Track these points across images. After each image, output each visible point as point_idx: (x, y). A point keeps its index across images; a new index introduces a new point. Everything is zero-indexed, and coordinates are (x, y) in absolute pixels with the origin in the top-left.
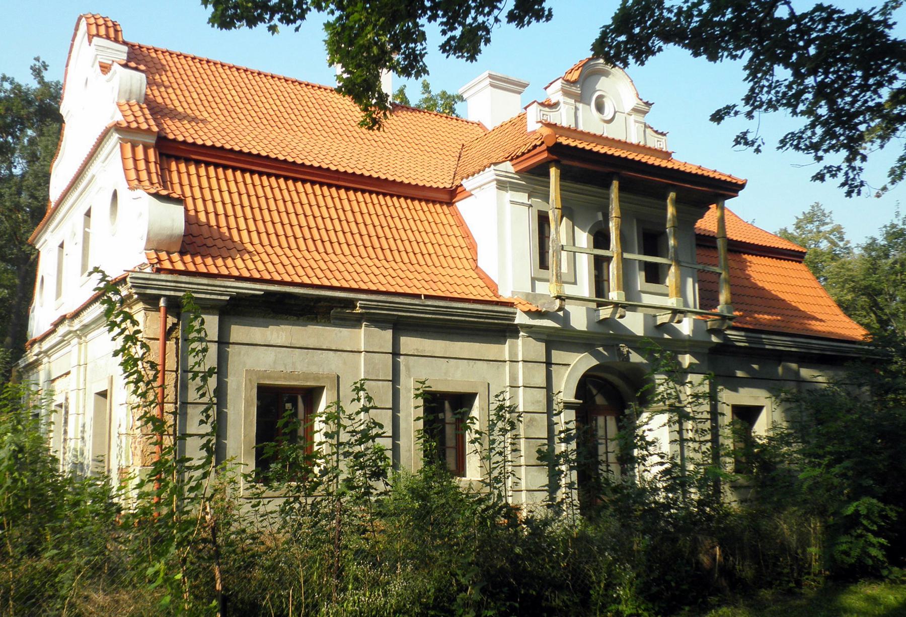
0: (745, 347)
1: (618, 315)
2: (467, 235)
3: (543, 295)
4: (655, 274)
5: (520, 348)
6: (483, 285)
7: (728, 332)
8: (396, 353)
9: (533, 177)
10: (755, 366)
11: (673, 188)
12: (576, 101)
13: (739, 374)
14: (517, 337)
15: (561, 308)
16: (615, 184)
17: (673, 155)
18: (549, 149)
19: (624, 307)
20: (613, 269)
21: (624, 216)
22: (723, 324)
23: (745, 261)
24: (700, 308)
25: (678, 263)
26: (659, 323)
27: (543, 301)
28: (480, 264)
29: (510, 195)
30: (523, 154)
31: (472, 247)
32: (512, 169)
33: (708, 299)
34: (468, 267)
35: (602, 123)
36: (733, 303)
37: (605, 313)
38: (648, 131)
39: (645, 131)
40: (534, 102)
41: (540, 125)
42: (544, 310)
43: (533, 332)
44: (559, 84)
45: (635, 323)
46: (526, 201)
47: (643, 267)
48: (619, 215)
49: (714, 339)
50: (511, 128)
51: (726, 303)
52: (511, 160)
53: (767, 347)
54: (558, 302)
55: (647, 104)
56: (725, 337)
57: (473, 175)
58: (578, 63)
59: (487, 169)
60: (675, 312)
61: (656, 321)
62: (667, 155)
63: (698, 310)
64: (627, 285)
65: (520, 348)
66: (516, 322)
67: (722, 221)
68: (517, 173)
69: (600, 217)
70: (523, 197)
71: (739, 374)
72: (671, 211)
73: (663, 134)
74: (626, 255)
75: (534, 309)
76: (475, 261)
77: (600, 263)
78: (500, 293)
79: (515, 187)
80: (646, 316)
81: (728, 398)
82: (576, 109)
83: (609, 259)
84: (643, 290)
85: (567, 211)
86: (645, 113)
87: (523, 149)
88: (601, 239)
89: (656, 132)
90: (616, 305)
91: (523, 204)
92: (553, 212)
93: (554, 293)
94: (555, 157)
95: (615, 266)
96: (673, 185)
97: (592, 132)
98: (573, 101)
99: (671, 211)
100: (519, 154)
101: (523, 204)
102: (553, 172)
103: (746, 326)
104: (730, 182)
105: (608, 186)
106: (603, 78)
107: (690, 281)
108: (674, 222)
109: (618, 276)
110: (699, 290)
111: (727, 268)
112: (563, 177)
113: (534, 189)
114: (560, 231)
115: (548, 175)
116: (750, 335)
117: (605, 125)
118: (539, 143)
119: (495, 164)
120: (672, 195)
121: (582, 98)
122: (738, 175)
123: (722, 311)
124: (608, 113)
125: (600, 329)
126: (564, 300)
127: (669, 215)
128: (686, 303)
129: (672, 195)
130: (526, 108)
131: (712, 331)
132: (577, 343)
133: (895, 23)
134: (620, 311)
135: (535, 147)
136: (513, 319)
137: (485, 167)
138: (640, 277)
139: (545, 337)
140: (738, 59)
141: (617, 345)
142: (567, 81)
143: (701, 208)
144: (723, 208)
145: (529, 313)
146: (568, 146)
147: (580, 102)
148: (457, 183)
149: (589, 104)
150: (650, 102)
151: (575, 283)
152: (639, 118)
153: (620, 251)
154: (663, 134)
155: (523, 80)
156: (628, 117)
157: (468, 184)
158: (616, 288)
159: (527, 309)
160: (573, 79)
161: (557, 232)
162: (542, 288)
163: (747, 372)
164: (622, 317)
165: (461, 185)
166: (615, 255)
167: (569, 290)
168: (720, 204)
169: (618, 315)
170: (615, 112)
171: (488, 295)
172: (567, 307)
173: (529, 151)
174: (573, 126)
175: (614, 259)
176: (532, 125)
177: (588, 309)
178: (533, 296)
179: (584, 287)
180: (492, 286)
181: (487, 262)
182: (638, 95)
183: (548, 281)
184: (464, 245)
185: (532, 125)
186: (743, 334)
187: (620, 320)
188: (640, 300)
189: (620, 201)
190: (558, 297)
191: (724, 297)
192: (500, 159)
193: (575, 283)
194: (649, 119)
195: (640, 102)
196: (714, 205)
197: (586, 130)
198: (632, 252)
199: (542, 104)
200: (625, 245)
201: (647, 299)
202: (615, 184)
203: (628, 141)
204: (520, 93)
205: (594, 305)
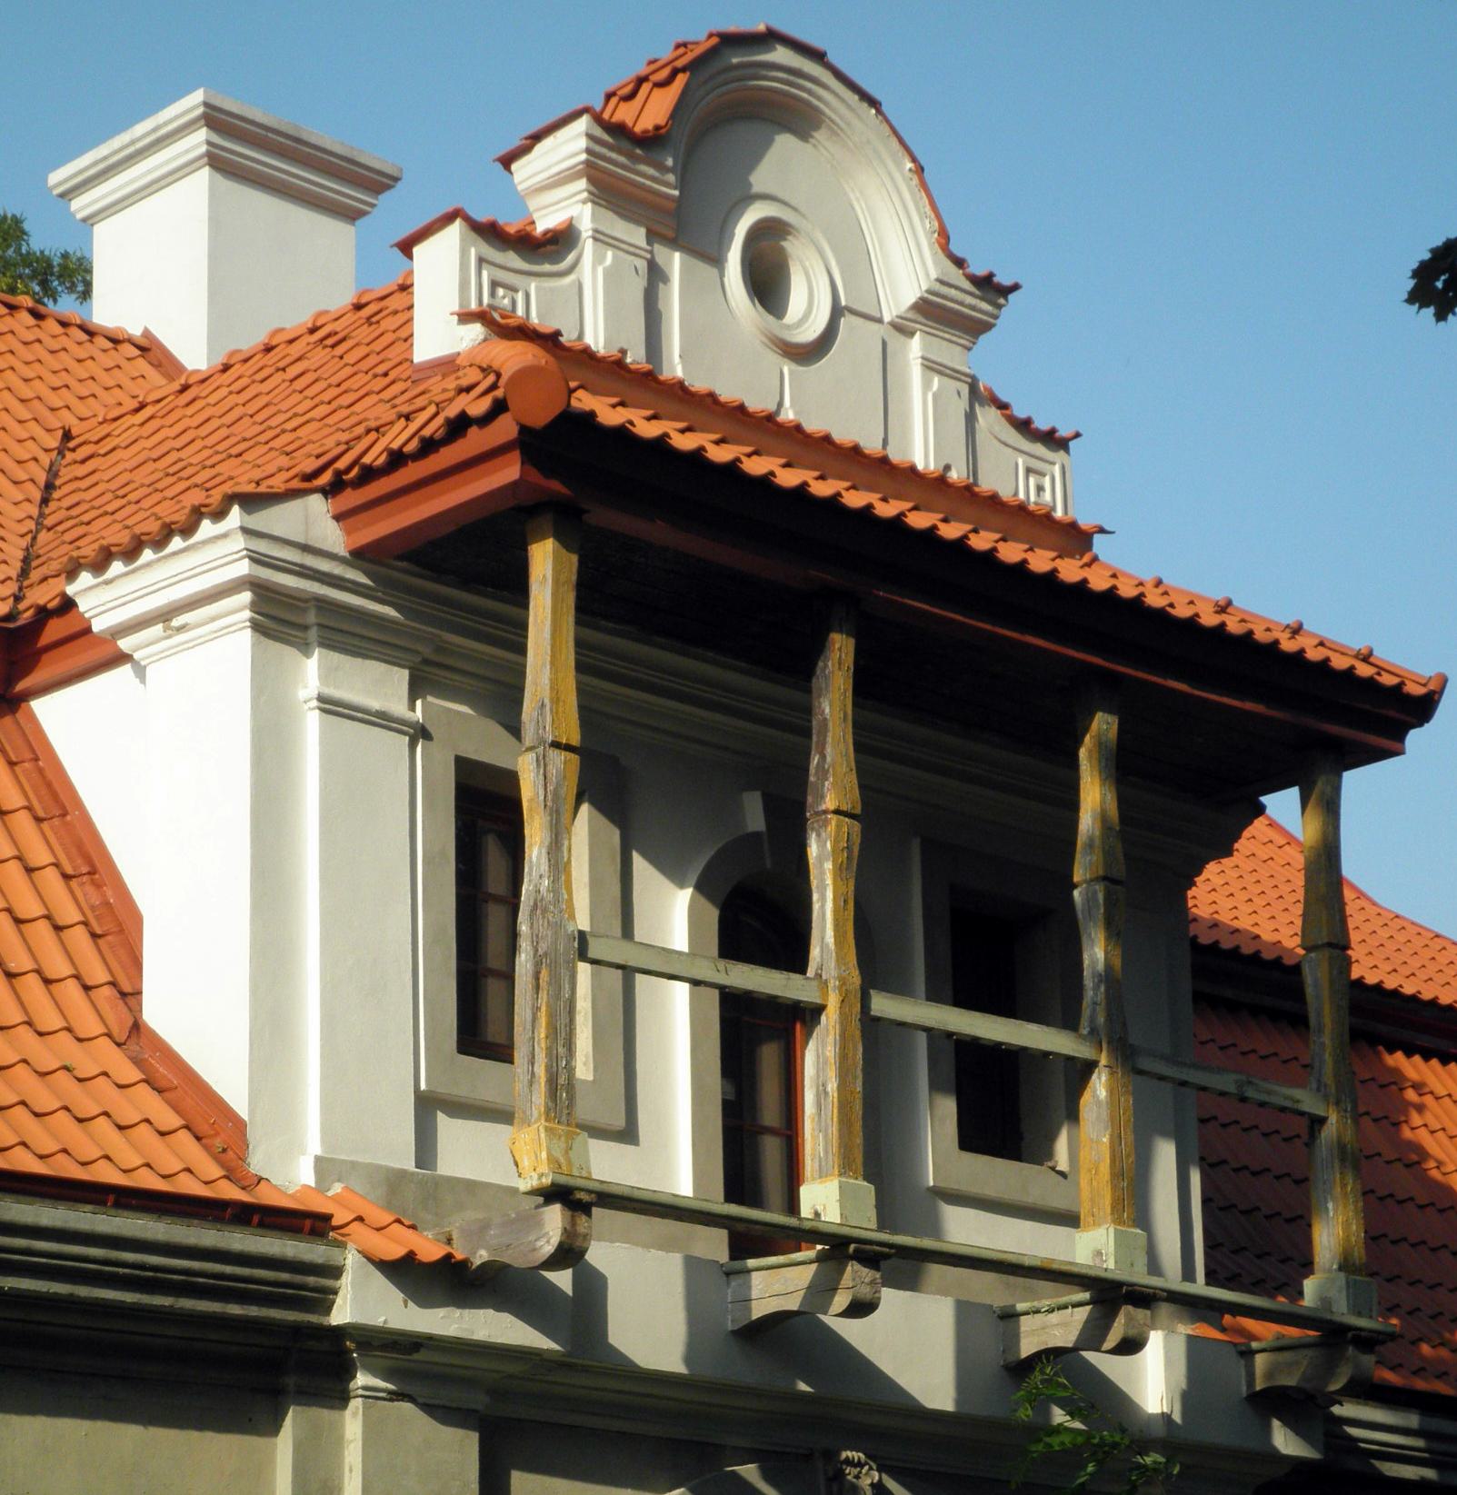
0: (1422, 1484)
1: (841, 1301)
2: (89, 864)
3: (471, 1186)
4: (1005, 1110)
5: (353, 1455)
6: (170, 1120)
9: (427, 581)
11: (1113, 692)
12: (652, 236)
14: (339, 1398)
15: (569, 1254)
16: (840, 652)
17: (1099, 542)
18: (531, 443)
19: (872, 1256)
20: (821, 1063)
21: (877, 818)
22: (1329, 1370)
23: (1396, 1081)
24: (1212, 1278)
25: (1127, 1056)
26: (1027, 1348)
27: (472, 1215)
28: (154, 1013)
29: (312, 672)
30: (397, 459)
31: (116, 927)
32: (333, 537)
33: (1250, 1239)
34: (91, 1026)
35: (773, 359)
36: (1373, 1264)
37: (776, 1286)
38: (988, 418)
39: (970, 418)
40: (448, 219)
41: (476, 331)
42: (481, 1256)
43: (421, 1372)
44: (571, 144)
45: (913, 1346)
46: (399, 707)
47: (961, 1072)
48: (852, 800)
49: (1285, 1441)
50: (320, 355)
51: (1346, 1265)
52: (331, 491)
54: (554, 1219)
55: (988, 286)
56: (1333, 1435)
57: (131, 554)
58: (665, 53)
59: (207, 528)
60: (1109, 1296)
61: (1013, 1338)
62: (1076, 538)
63: (1200, 1287)
64: (878, 1151)
65: (353, 1455)
66: (342, 1314)
67: (1325, 865)
68: (360, 556)
69: (754, 817)
70: (383, 686)
72: (1094, 797)
73: (1053, 440)
74: (883, 1005)
75: (430, 1250)
76: (130, 996)
77: (750, 1040)
78: (258, 1162)
79: (344, 633)
80: (965, 1311)
82: (656, 275)
83: (808, 1015)
84: (950, 1184)
85: (605, 779)
86: (974, 328)
87: (398, 437)
88: (758, 917)
89: (1024, 426)
90: (839, 1249)
91: (383, 720)
92: (542, 762)
93: (535, 1174)
94: (556, 486)
95: (831, 1052)
96: (1111, 681)
97: (727, 393)
98: (638, 236)
99: (1094, 797)
100: (376, 457)
101: (383, 720)
102: (546, 563)
103: (1421, 1384)
104: (1370, 683)
105: (800, 667)
106: (784, 143)
107: (1166, 1154)
108: (1108, 854)
109: (844, 1106)
110: (1206, 1201)
111: (1346, 1093)
112: (593, 601)
113: (440, 649)
114: (566, 857)
115: (516, 586)
117: (787, 368)
118: (479, 408)
119: (251, 501)
120: (1103, 725)
121: (684, 224)
122: (1410, 653)
123: (1326, 1302)
124: (806, 308)
125: (746, 1370)
126: (585, 1208)
127: (1087, 822)
128: (1154, 1267)
129: (1103, 725)
130: (406, 247)
131: (1272, 1402)
134: (855, 1277)
135: (459, 425)
136: (324, 1299)
137: (197, 514)
138: (937, 1123)
139: (479, 1401)
141: (830, 1455)
142: (618, 131)
143: (1224, 813)
144: (1331, 809)
145: (406, 1272)
146: (622, 434)
147: (673, 243)
148: (42, 595)
149: (716, 260)
150: (1003, 279)
151: (628, 1134)
152: (951, 354)
153: (855, 979)
154: (1053, 440)
155: (375, 155)
156: (895, 340)
157: (102, 600)
158: (833, 1161)
159: (395, 1252)
160: (646, 124)
161: (559, 867)
162: (469, 1151)
164: (861, 1308)
165: (68, 605)
166: (833, 1003)
167: (607, 1165)
168: (1321, 785)
169: (841, 1301)
170: (837, 312)
171: (199, 1175)
172: (598, 1255)
173: (429, 446)
174: (636, 356)
175: (830, 1019)
176: (439, 332)
177: (693, 1266)
178: (419, 1189)
179: (674, 1151)
180: (214, 1125)
181: (195, 1000)
182: (944, 237)
183: (503, 1116)
184: (69, 914)
185: (439, 332)
186: (1413, 1420)
187: (852, 1331)
188: (935, 1229)
189: (861, 747)
190: (557, 1194)
191: (1333, 1232)
192: (278, 483)
193: (628, 1134)
194: (989, 359)
195: (956, 275)
196: (1293, 794)
197: (699, 383)
198: (900, 988)
199: (490, 232)
200: (875, 960)
201: (965, 1229)
202: (840, 652)
203: (895, 456)
204: (351, 215)
205: (714, 1245)
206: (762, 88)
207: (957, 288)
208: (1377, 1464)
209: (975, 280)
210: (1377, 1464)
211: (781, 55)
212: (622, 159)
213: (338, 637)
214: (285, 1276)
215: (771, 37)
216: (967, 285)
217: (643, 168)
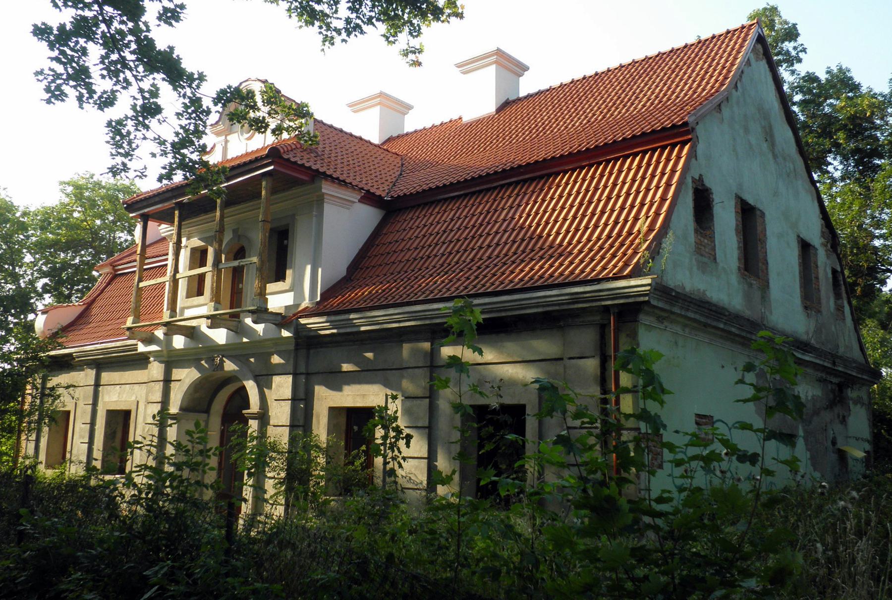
0: (332, 334)
7: (303, 321)
8: (97, 385)
10: (370, 355)
13: (346, 367)
53: (363, 329)
71: (346, 367)
81: (326, 399)
116: (333, 318)
132: (189, 360)
133: (290, 16)
140: (313, 32)
163: (356, 364)
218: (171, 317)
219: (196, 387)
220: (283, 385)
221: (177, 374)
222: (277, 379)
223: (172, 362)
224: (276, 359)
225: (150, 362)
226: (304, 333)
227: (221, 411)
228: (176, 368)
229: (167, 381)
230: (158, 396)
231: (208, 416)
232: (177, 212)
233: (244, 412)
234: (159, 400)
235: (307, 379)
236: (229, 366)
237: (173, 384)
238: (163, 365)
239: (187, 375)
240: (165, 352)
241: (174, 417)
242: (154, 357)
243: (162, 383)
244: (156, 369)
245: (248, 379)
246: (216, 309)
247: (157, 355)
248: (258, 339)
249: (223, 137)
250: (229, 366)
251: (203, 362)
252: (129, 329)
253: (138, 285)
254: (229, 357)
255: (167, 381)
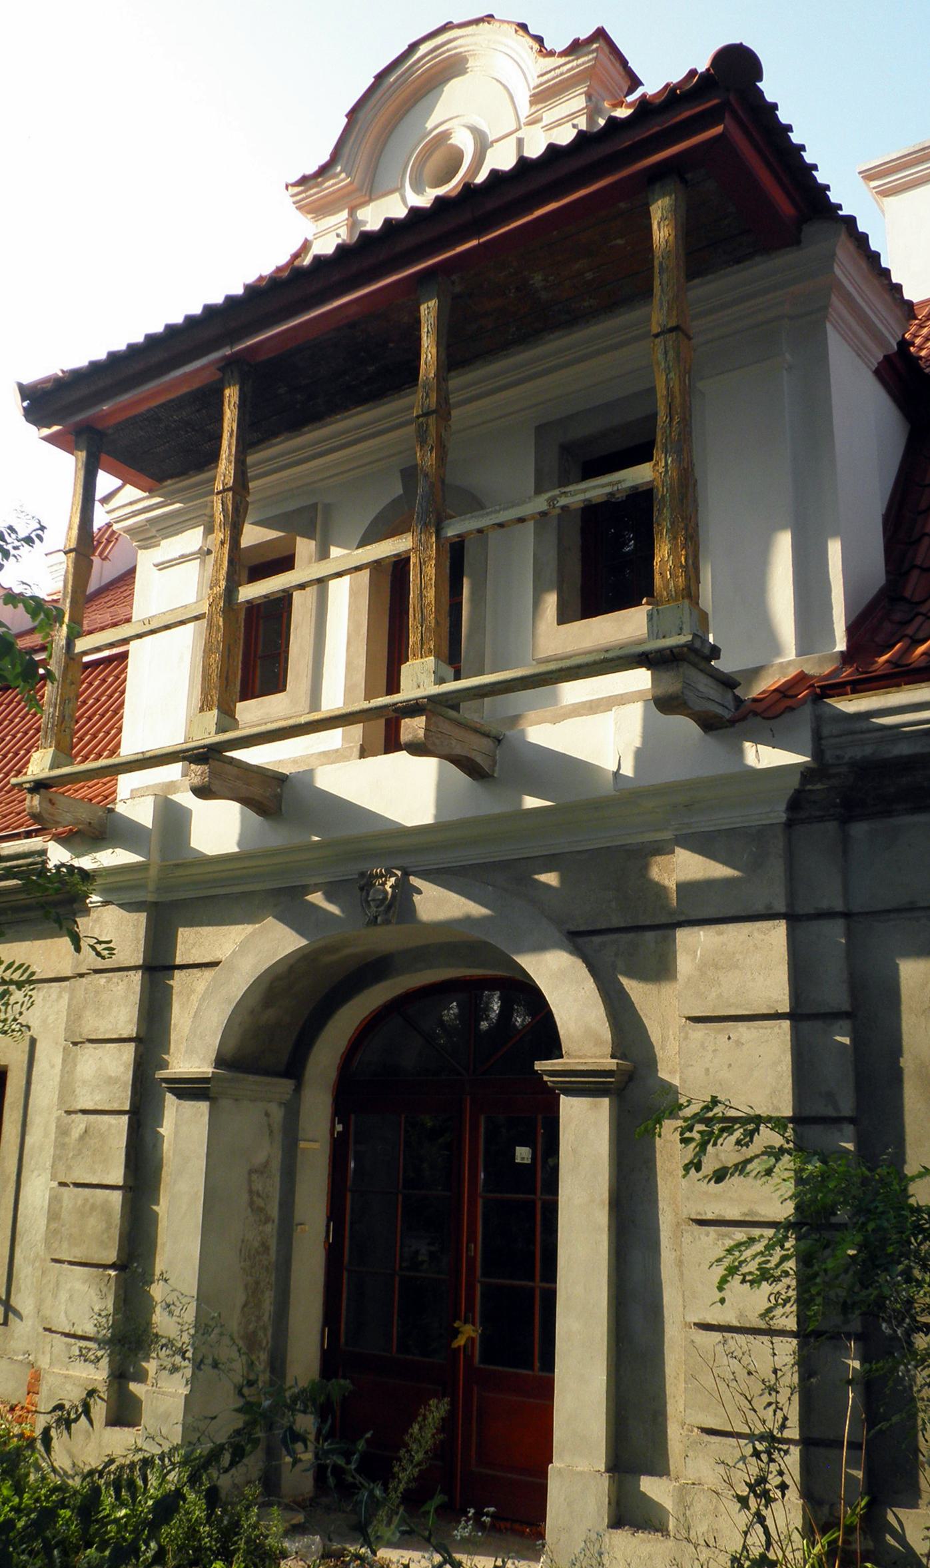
206: (419, 76)
207: (559, 67)
208: (237, 754)
209: (565, 53)
210: (237, 754)
211: (424, 48)
212: (315, 190)
213: (165, 531)
214: (30, 860)
215: (413, 47)
216: (564, 60)
217: (327, 184)
218: (221, 729)
219: (276, 986)
220: (750, 962)
221: (193, 943)
222: (694, 946)
223: (175, 905)
224: (682, 868)
225: (86, 911)
226: (856, 753)
227: (333, 1074)
228: (191, 923)
229: (158, 968)
230: (122, 1016)
231: (298, 1089)
232: (231, 394)
233: (539, 1066)
234: (130, 1030)
235: (849, 934)
236: (438, 904)
237: (179, 980)
238: (142, 917)
239: (243, 948)
240: (153, 872)
241: (190, 1089)
242: (103, 891)
243: (137, 977)
244: (116, 928)
245: (540, 947)
246: (440, 680)
247: (120, 888)
248: (608, 788)
249: (344, 214)
250: (438, 904)
251: (317, 898)
252: (40, 786)
253: (70, 644)
254: (432, 875)
255: (158, 968)
